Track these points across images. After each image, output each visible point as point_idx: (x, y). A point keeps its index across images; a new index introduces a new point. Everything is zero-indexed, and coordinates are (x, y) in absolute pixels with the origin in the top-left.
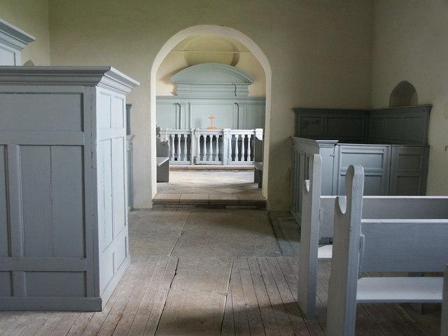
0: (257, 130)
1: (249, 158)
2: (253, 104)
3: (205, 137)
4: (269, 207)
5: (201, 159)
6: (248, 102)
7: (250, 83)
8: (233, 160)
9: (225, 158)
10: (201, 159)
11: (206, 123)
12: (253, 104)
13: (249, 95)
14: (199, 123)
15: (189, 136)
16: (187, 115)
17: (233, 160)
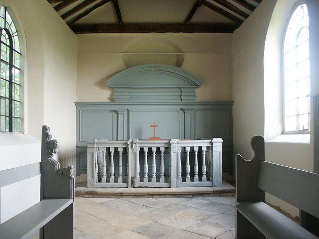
0: (215, 140)
1: (205, 176)
2: (201, 110)
3: (112, 150)
5: (142, 181)
6: (195, 107)
7: (197, 86)
8: (184, 180)
9: (173, 178)
10: (142, 181)
11: (148, 133)
12: (201, 110)
13: (197, 99)
14: (139, 134)
15: (125, 151)
16: (126, 123)
17: (184, 180)
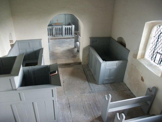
4: (82, 64)
5: (56, 35)
8: (66, 35)
9: (63, 34)
10: (56, 35)
17: (66, 35)
